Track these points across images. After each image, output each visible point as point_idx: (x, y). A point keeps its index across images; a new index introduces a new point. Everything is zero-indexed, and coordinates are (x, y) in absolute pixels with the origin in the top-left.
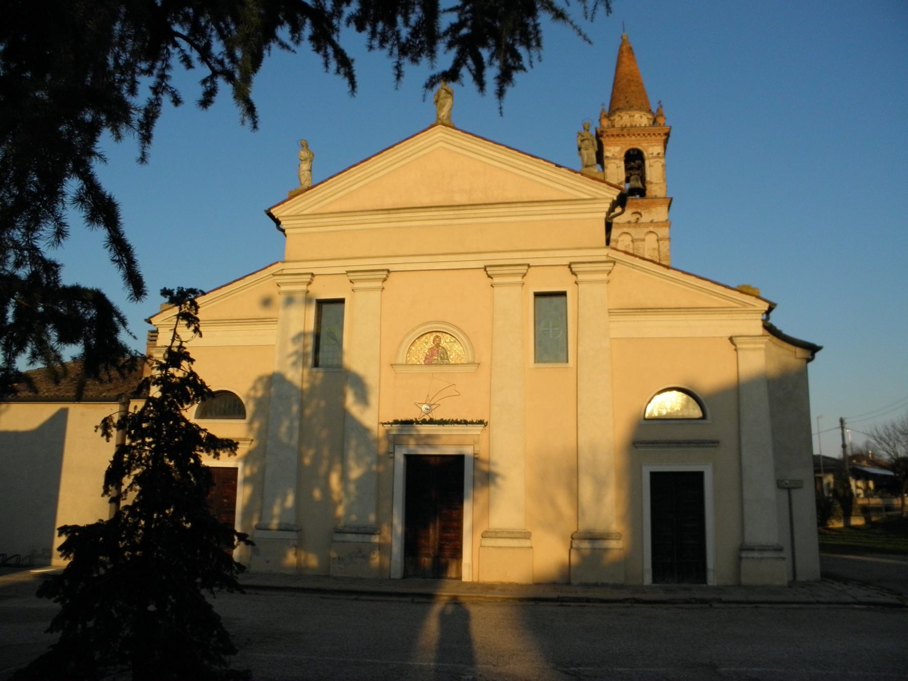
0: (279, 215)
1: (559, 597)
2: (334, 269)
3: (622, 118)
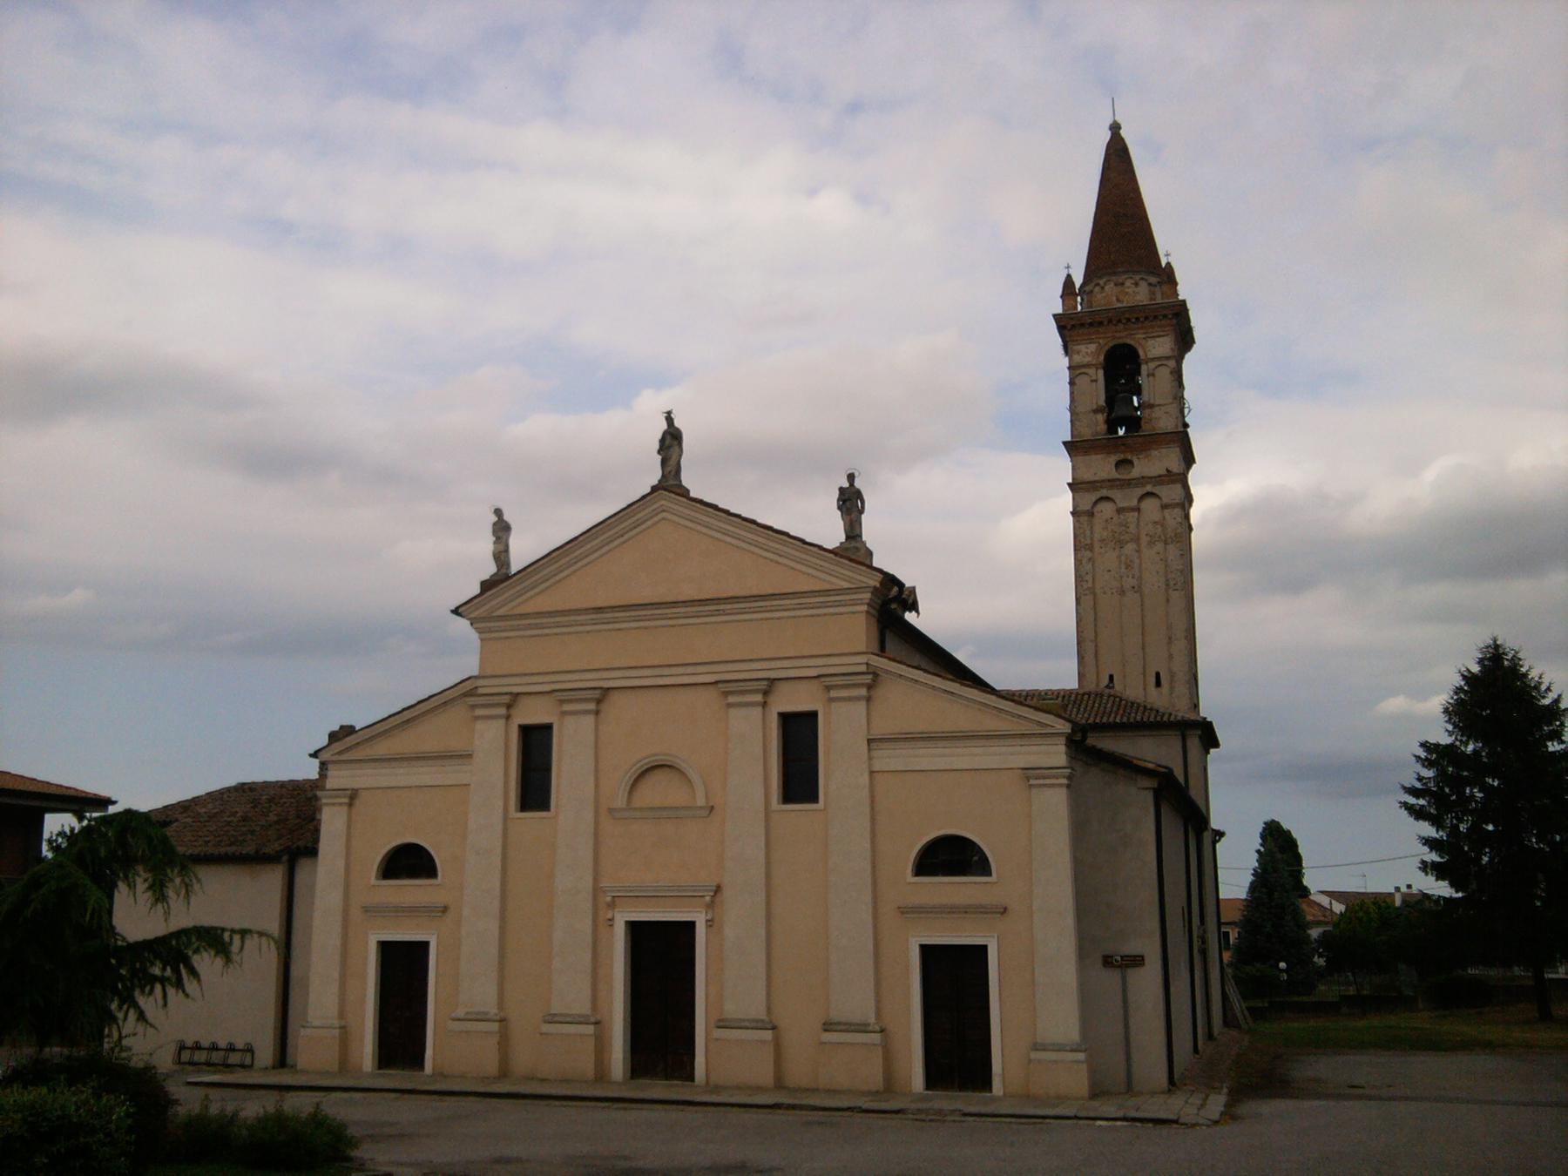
3: (1103, 288)
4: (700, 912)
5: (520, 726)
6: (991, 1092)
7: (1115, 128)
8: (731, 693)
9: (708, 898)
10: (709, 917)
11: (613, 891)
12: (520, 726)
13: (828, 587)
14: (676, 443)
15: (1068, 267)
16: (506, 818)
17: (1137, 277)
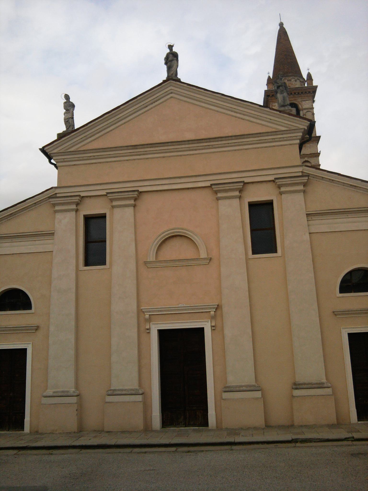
0: (51, 152)
1: (293, 440)
2: (97, 191)
5: (84, 216)
7: (281, 25)
8: (220, 191)
9: (212, 313)
10: (213, 324)
11: (150, 312)
12: (84, 216)
14: (175, 59)
15: (269, 73)
17: (296, 78)
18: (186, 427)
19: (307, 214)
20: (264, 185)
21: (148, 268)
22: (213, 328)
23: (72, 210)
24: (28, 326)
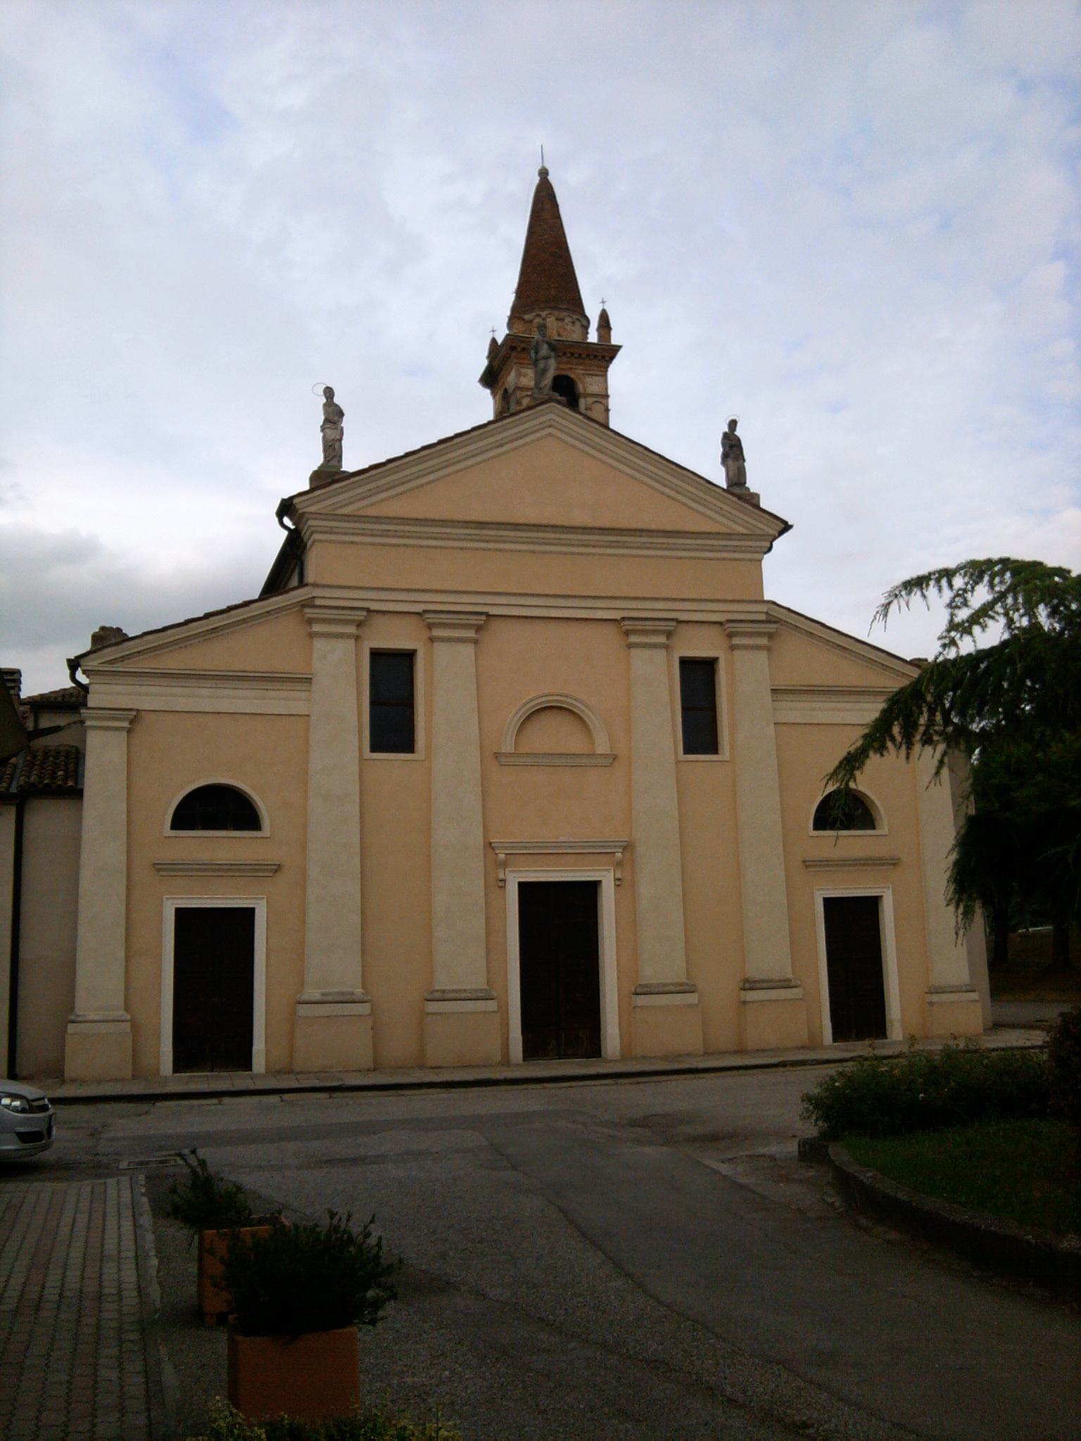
0: (305, 510)
4: (608, 871)
6: (251, 1070)
7: (544, 173)
8: (635, 632)
10: (619, 876)
11: (506, 848)
13: (724, 530)
16: (362, 760)
17: (575, 317)
18: (559, 1059)
19: (771, 690)
20: (705, 630)
21: (501, 765)
22: (618, 883)
23: (349, 636)
24: (257, 862)
